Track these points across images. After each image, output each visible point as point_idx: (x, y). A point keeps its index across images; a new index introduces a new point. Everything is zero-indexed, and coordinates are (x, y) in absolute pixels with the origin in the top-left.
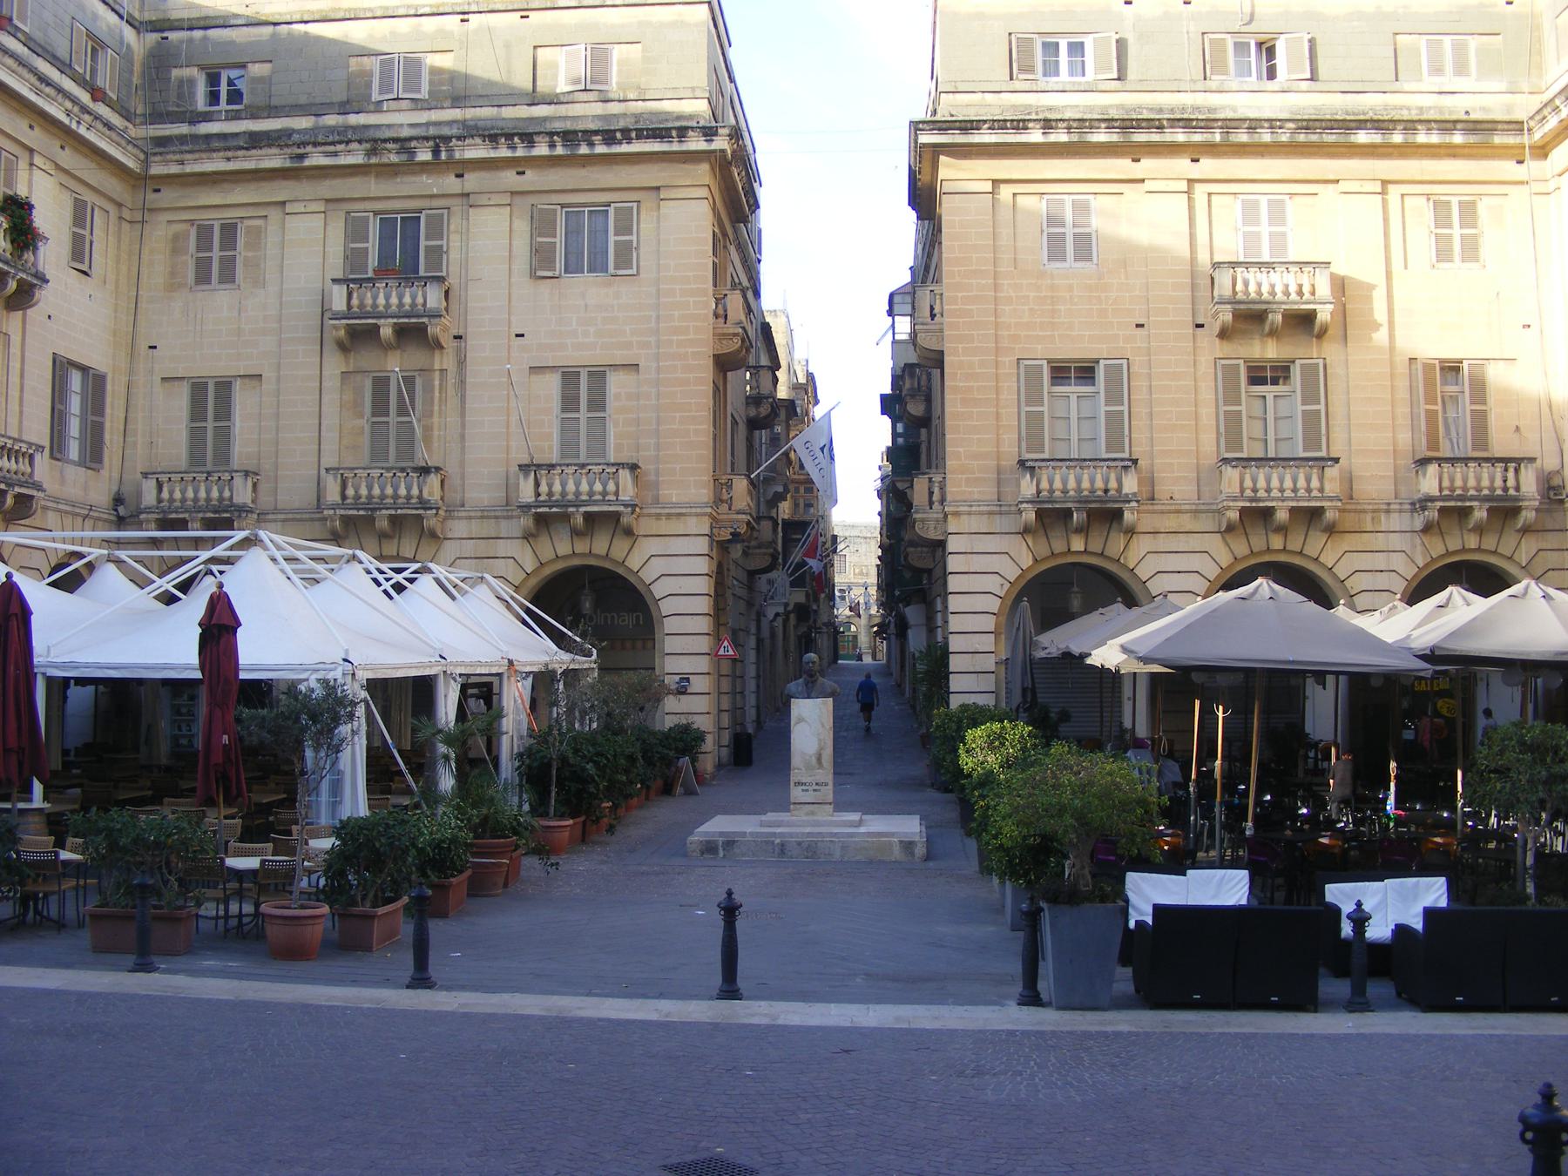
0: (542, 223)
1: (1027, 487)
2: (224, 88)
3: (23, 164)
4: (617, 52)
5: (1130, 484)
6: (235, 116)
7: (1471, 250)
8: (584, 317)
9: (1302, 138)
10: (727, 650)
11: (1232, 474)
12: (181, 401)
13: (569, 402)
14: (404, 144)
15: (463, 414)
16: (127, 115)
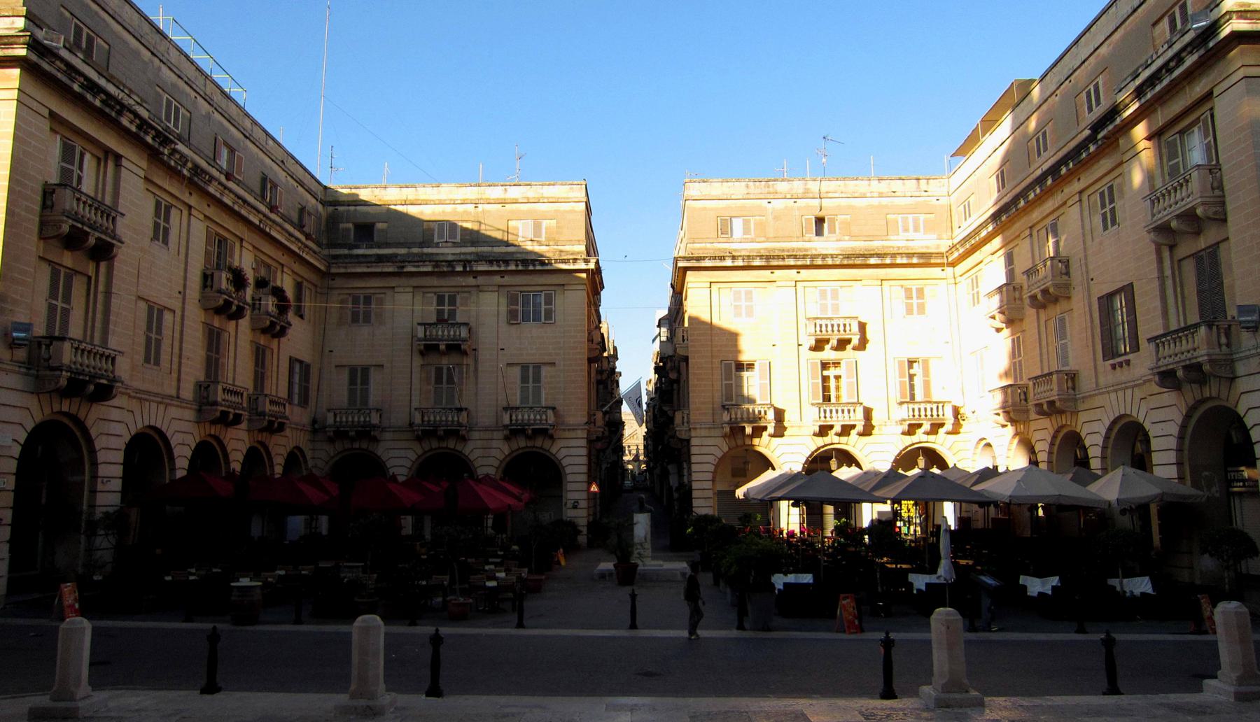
0: (512, 300)
1: (726, 417)
4: (545, 223)
7: (921, 309)
8: (531, 341)
9: (845, 262)
10: (594, 488)
13: (524, 379)
14: (450, 263)
15: (477, 384)
16: (319, 245)
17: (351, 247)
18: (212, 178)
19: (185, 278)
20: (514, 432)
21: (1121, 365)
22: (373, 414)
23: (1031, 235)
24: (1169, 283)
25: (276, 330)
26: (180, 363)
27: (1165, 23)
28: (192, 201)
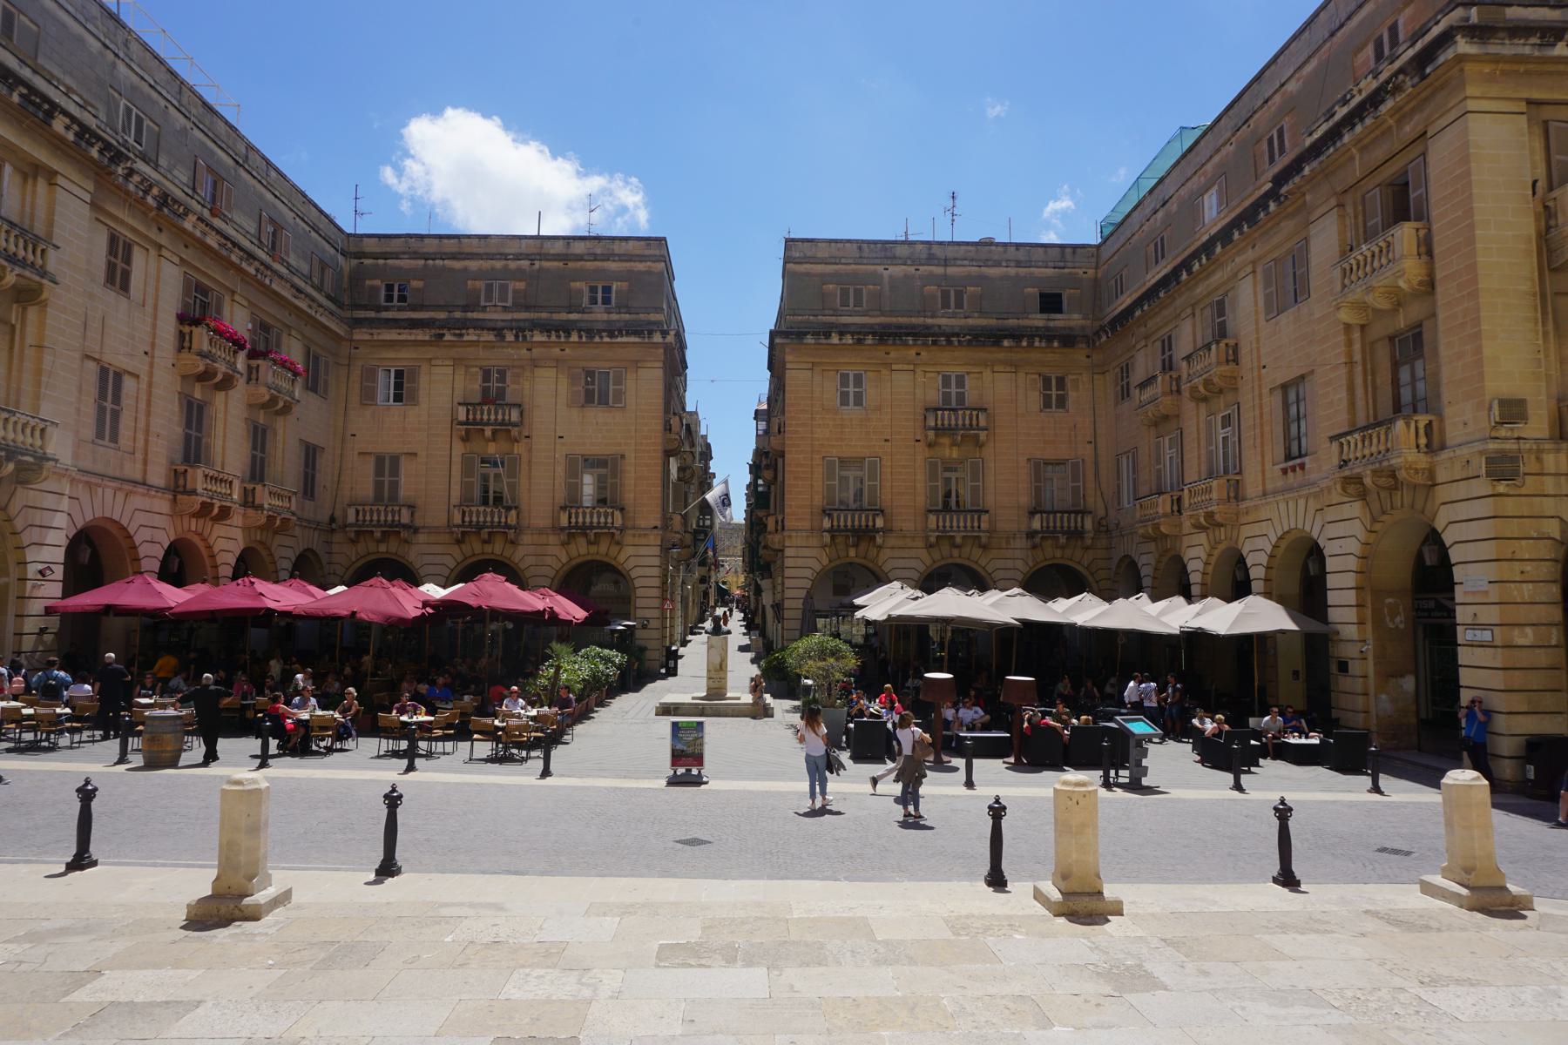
2: (396, 294)
3: (227, 298)
5: (880, 523)
6: (400, 309)
7: (1062, 402)
8: (597, 431)
11: (932, 518)
12: (370, 466)
16: (341, 306)
17: (378, 309)
18: (187, 211)
19: (154, 336)
20: (573, 532)
21: (1293, 469)
22: (404, 511)
23: (1254, 272)
24: (1359, 369)
25: (277, 407)
26: (146, 441)
27: (1370, 50)
28: (163, 239)
